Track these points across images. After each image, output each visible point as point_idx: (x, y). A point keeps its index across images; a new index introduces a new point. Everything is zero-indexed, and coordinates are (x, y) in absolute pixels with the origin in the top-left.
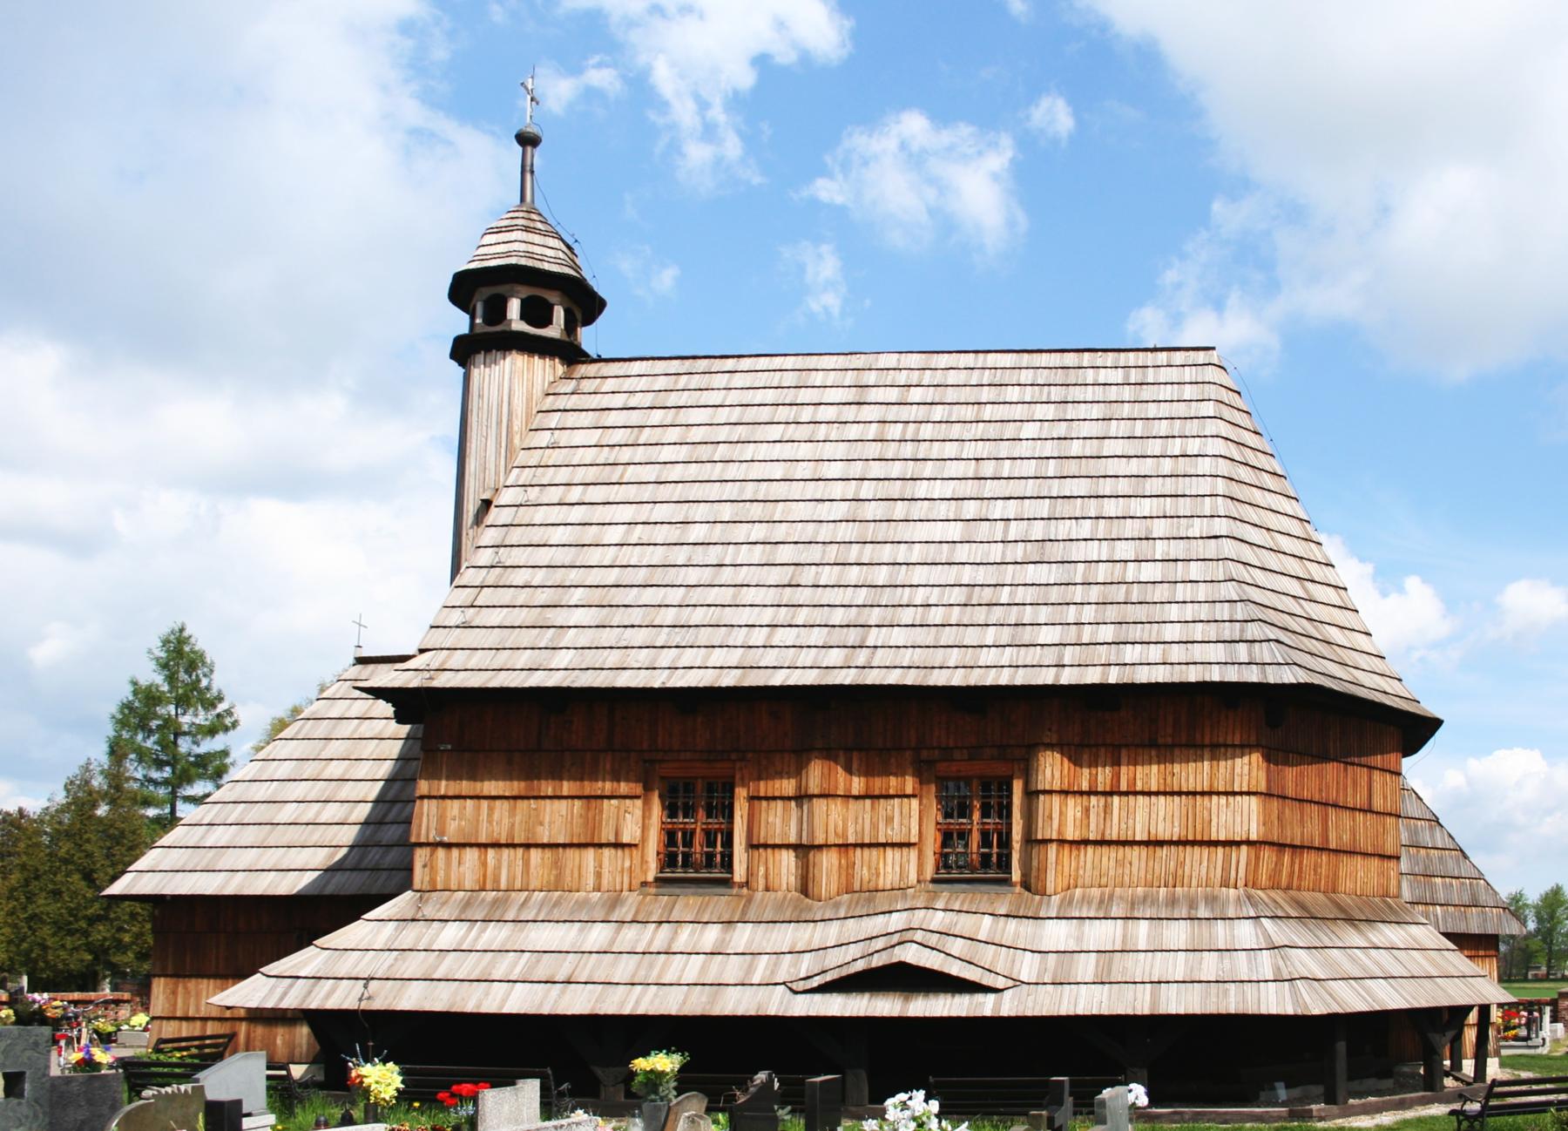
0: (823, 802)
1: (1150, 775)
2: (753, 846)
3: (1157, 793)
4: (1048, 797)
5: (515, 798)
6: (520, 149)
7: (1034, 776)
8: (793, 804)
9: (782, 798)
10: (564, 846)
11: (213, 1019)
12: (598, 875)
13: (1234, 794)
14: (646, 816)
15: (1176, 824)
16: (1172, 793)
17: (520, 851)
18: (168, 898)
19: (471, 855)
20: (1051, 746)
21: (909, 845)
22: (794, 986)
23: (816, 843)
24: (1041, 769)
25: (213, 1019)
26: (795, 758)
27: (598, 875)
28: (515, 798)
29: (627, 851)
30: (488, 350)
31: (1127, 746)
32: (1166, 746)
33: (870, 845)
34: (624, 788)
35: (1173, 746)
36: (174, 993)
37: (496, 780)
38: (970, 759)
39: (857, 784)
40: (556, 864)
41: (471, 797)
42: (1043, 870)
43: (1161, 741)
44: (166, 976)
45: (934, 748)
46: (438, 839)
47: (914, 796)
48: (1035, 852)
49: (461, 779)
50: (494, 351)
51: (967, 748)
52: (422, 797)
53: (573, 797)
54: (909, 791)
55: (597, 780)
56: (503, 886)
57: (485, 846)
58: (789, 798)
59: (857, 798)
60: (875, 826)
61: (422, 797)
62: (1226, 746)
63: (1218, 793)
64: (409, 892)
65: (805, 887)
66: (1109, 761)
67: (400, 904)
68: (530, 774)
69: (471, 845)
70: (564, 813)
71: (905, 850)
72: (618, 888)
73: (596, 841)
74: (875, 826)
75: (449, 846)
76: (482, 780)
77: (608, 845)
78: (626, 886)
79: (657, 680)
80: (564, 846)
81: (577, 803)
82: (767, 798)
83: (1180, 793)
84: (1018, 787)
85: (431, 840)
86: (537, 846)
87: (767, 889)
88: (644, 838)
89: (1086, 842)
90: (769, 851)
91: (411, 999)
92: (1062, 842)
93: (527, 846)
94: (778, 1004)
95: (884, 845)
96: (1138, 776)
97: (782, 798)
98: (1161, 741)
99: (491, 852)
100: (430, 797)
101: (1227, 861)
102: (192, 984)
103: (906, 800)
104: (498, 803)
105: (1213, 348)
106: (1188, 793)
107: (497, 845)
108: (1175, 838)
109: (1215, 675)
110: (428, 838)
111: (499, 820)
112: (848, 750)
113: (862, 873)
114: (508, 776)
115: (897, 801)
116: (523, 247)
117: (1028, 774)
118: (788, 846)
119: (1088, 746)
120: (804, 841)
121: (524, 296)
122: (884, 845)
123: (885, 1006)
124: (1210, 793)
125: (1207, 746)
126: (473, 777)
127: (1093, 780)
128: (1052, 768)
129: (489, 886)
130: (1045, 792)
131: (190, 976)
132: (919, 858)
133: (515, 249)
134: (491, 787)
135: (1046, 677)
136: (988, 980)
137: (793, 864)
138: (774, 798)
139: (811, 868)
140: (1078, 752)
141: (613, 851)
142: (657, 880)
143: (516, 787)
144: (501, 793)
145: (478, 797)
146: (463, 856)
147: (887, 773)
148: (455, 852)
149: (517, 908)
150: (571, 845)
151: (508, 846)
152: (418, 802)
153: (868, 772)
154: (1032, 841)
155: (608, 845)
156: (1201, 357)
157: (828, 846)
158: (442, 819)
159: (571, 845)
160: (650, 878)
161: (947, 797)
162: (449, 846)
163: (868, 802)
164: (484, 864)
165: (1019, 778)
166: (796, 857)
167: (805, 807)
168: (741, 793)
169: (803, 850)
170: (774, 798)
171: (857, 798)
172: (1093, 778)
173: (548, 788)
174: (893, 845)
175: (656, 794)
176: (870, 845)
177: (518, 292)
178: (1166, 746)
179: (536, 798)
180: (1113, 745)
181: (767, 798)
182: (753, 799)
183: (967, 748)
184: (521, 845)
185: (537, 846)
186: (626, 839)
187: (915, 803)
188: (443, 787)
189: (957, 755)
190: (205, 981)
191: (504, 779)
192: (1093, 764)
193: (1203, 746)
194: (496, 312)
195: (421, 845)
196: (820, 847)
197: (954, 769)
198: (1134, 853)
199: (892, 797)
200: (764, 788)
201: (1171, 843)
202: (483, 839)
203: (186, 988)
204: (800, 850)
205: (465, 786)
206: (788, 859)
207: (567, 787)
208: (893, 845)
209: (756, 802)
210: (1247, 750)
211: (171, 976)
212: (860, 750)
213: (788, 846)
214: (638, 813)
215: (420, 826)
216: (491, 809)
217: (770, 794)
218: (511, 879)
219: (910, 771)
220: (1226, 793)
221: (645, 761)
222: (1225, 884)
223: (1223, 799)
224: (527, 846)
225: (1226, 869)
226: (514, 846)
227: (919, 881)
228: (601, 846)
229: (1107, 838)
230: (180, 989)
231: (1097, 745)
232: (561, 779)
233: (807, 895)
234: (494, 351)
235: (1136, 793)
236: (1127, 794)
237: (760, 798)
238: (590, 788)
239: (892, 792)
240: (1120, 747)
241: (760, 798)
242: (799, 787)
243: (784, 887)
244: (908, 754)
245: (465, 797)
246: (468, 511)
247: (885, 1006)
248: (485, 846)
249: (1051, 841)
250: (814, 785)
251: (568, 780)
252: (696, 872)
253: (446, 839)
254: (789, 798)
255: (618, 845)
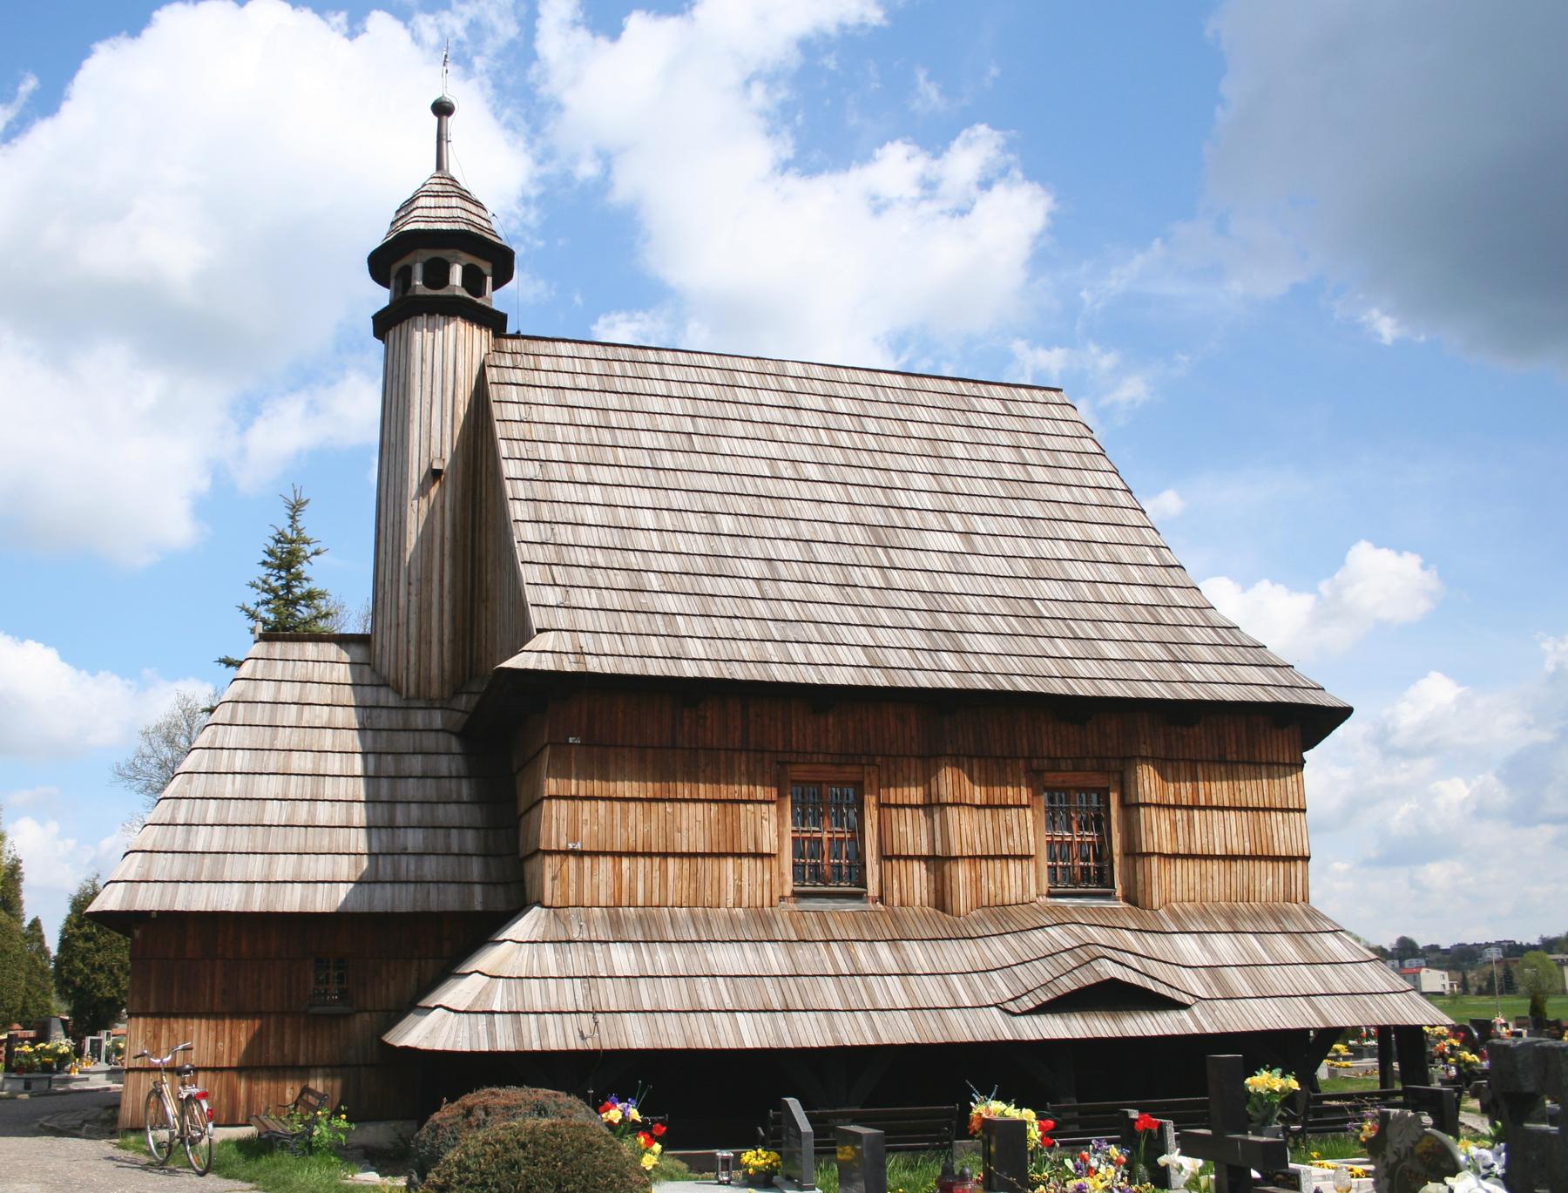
0: (955, 809)
1: (1220, 791)
2: (885, 857)
3: (1229, 809)
4: (1147, 809)
5: (649, 800)
6: (436, 119)
7: (1133, 789)
8: (921, 812)
9: (911, 806)
10: (704, 855)
11: (205, 1069)
12: (739, 889)
13: (1288, 810)
14: (781, 823)
15: (1246, 839)
16: (1240, 809)
17: (657, 861)
18: (154, 915)
19: (605, 864)
20: (1145, 759)
21: (1028, 857)
22: (1012, 1006)
23: (953, 854)
24: (1139, 781)
25: (205, 1069)
26: (926, 767)
27: (739, 889)
28: (649, 800)
29: (766, 861)
30: (431, 313)
31: (1202, 761)
32: (1232, 762)
33: (994, 857)
34: (760, 792)
35: (1237, 762)
36: (156, 1037)
37: (631, 780)
38: (1075, 770)
39: (979, 794)
40: (694, 875)
41: (603, 799)
42: (1148, 883)
43: (1229, 757)
44: (145, 1015)
45: (1043, 758)
46: (571, 846)
47: (1028, 806)
48: (1138, 866)
49: (592, 779)
50: (437, 315)
51: (1071, 759)
52: (550, 798)
53: (709, 801)
54: (1025, 802)
55: (733, 784)
56: (640, 902)
57: (620, 854)
58: (917, 806)
59: (978, 807)
60: (997, 838)
61: (550, 798)
62: (1278, 764)
63: (1276, 810)
64: (536, 909)
65: (941, 900)
66: (1188, 777)
67: (524, 926)
68: (664, 774)
69: (605, 854)
70: (700, 818)
71: (1025, 863)
72: (759, 903)
73: (736, 851)
74: (997, 838)
75: (580, 854)
76: (615, 780)
77: (748, 855)
78: (767, 902)
79: (811, 676)
80: (704, 855)
81: (714, 807)
82: (897, 806)
83: (1246, 809)
84: (1114, 799)
85: (563, 847)
86: (674, 855)
87: (902, 905)
88: (780, 849)
89: (1175, 856)
90: (902, 862)
91: (636, 1035)
92: (1161, 855)
93: (665, 855)
94: (997, 1028)
95: (1006, 857)
96: (1213, 791)
97: (911, 806)
98: (1229, 757)
99: (625, 862)
100: (558, 797)
101: (1288, 876)
102: (178, 1025)
103: (1021, 810)
104: (632, 805)
105: (1061, 390)
106: (1253, 809)
107: (632, 854)
108: (1247, 853)
109: (1148, 691)
110: (558, 844)
111: (636, 825)
112: (970, 757)
113: (988, 886)
114: (640, 776)
115: (1014, 811)
116: (464, 214)
117: (1125, 786)
118: (919, 858)
119: (1171, 760)
120: (939, 852)
121: (465, 264)
122: (1006, 857)
123: (1100, 1026)
124: (1269, 809)
125: (1263, 764)
126: (605, 777)
127: (1177, 794)
128: (1148, 782)
129: (625, 902)
130: (1145, 805)
131: (176, 1015)
132: (1036, 867)
133: (437, 216)
134: (625, 788)
135: (655, 669)
136: (1179, 997)
137: (924, 871)
138: (903, 806)
139: (948, 882)
140: (1169, 767)
141: (752, 861)
142: (795, 894)
143: (650, 789)
144: (636, 795)
145: (610, 799)
146: (596, 866)
147: (1003, 783)
148: (587, 861)
149: (670, 926)
150: (711, 855)
151: (643, 854)
152: (545, 802)
153: (987, 782)
154: (1134, 853)
155: (748, 855)
156: (1053, 396)
157: (962, 857)
158: (574, 822)
159: (711, 855)
160: (788, 892)
161: (1087, 808)
162: (580, 854)
163: (988, 811)
164: (618, 876)
165: (1113, 791)
166: (927, 869)
167: (937, 817)
168: (870, 800)
169: (938, 862)
170: (903, 806)
171: (978, 807)
172: (1177, 791)
173: (683, 790)
174: (1015, 857)
175: (789, 799)
176: (994, 857)
177: (460, 259)
178: (1232, 762)
179: (671, 800)
180: (1191, 760)
181: (897, 806)
182: (882, 806)
183: (1071, 759)
184: (658, 854)
185: (674, 855)
186: (766, 850)
187: (1029, 812)
188: (573, 786)
189: (1063, 765)
190: (196, 1021)
191: (638, 780)
192: (1176, 779)
193: (1260, 764)
194: (437, 274)
195: (551, 853)
196: (956, 858)
197: (1060, 779)
198: (1215, 867)
199: (1010, 807)
200: (895, 795)
201: (1244, 857)
202: (617, 848)
203: (170, 1030)
204: (931, 862)
205: (597, 787)
206: (919, 870)
207: (703, 790)
208: (1015, 857)
209: (886, 810)
210: (1294, 769)
211: (153, 1015)
212: (979, 757)
213: (919, 858)
214: (774, 819)
215: (550, 830)
216: (625, 814)
217: (900, 802)
218: (649, 892)
219: (1023, 780)
220: (1282, 810)
221: (778, 763)
222: (1288, 899)
223: (1280, 815)
224: (665, 855)
225: (1288, 884)
226: (650, 855)
227: (1037, 896)
228: (740, 855)
229: (1193, 852)
230: (164, 1032)
231: (1177, 760)
232: (697, 782)
233: (944, 911)
234: (437, 315)
235: (1212, 808)
236: (1204, 808)
237: (889, 806)
238: (726, 791)
239: (1010, 802)
240: (1196, 761)
241: (889, 806)
242: (928, 794)
243: (918, 902)
244: (1021, 762)
245: (596, 799)
246: (412, 480)
247: (1100, 1026)
248: (620, 854)
249: (1153, 854)
250: (947, 794)
251: (705, 783)
252: (826, 885)
253: (578, 846)
254: (917, 806)
255: (758, 855)
